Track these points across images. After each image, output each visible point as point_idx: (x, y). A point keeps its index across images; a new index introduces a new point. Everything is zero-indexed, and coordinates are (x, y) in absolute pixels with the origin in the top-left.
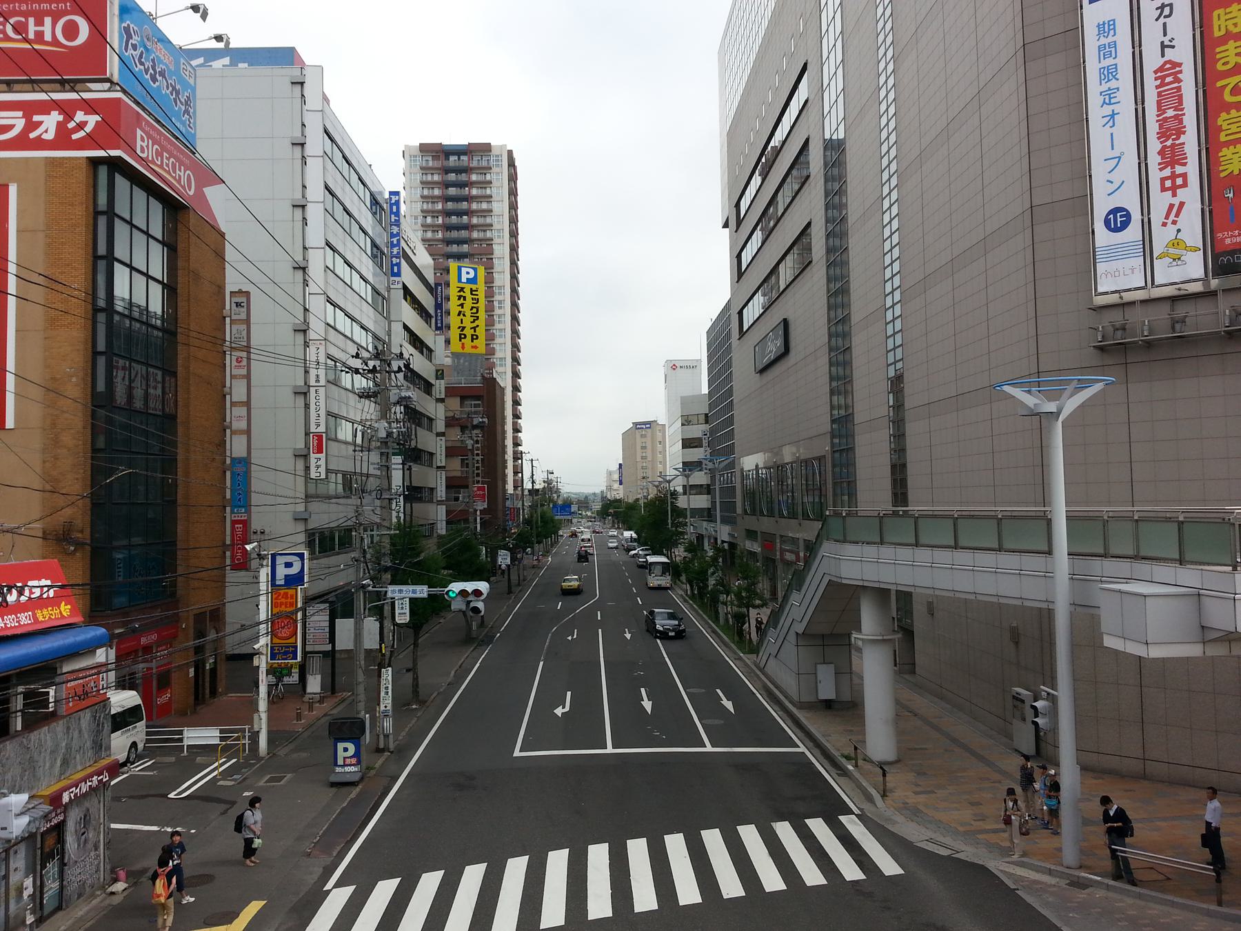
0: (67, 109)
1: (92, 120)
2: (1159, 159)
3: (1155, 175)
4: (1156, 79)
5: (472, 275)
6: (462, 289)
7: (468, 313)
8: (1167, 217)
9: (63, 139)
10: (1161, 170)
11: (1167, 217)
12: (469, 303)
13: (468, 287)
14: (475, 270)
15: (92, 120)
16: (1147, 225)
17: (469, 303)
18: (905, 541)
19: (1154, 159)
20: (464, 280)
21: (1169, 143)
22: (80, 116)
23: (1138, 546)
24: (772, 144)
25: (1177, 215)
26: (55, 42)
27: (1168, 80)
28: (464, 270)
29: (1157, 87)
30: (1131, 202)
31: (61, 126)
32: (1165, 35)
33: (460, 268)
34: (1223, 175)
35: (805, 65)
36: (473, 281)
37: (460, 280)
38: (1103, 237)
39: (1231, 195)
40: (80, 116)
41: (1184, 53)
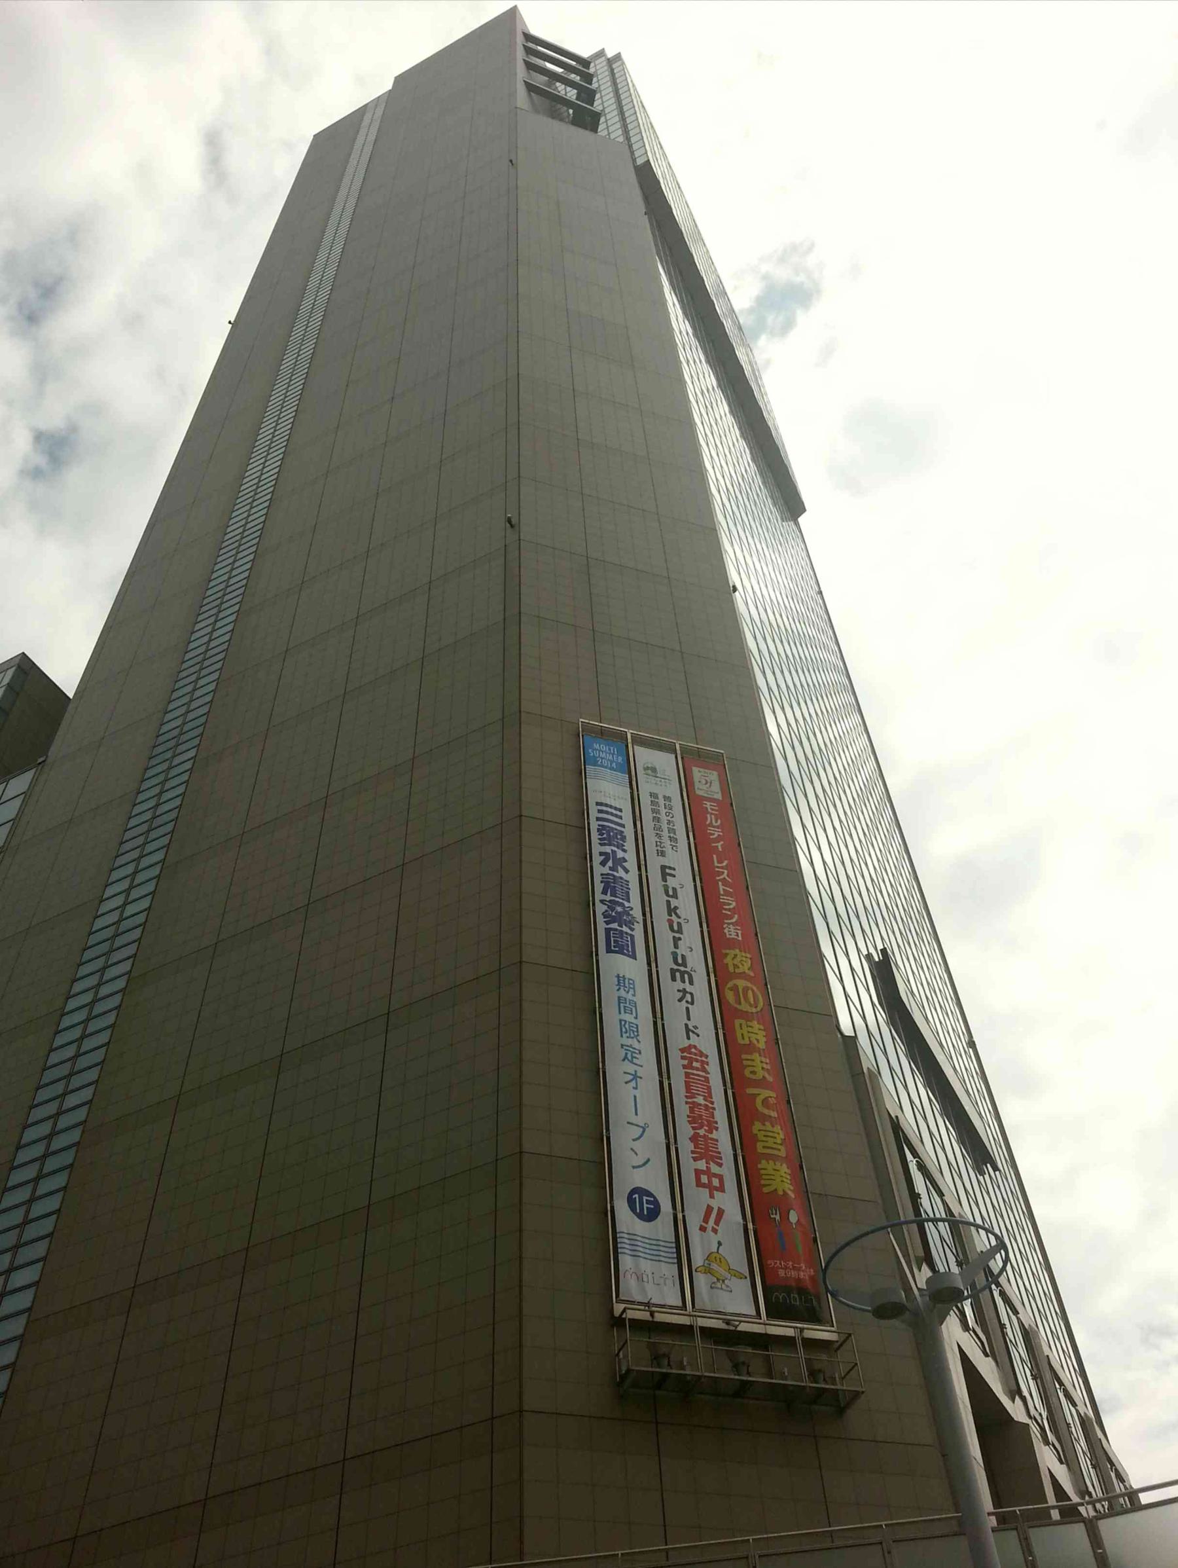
2: (691, 1146)
3: (689, 1166)
4: (683, 1058)
8: (706, 1220)
10: (695, 1159)
11: (706, 1220)
16: (679, 1224)
18: (790, 1549)
19: (686, 1147)
21: (702, 1132)
25: (717, 1222)
27: (695, 1064)
29: (684, 1067)
30: (656, 1182)
32: (689, 1019)
34: (766, 1190)
35: (648, 1160)
38: (626, 1220)
39: (778, 1217)
41: (706, 1042)
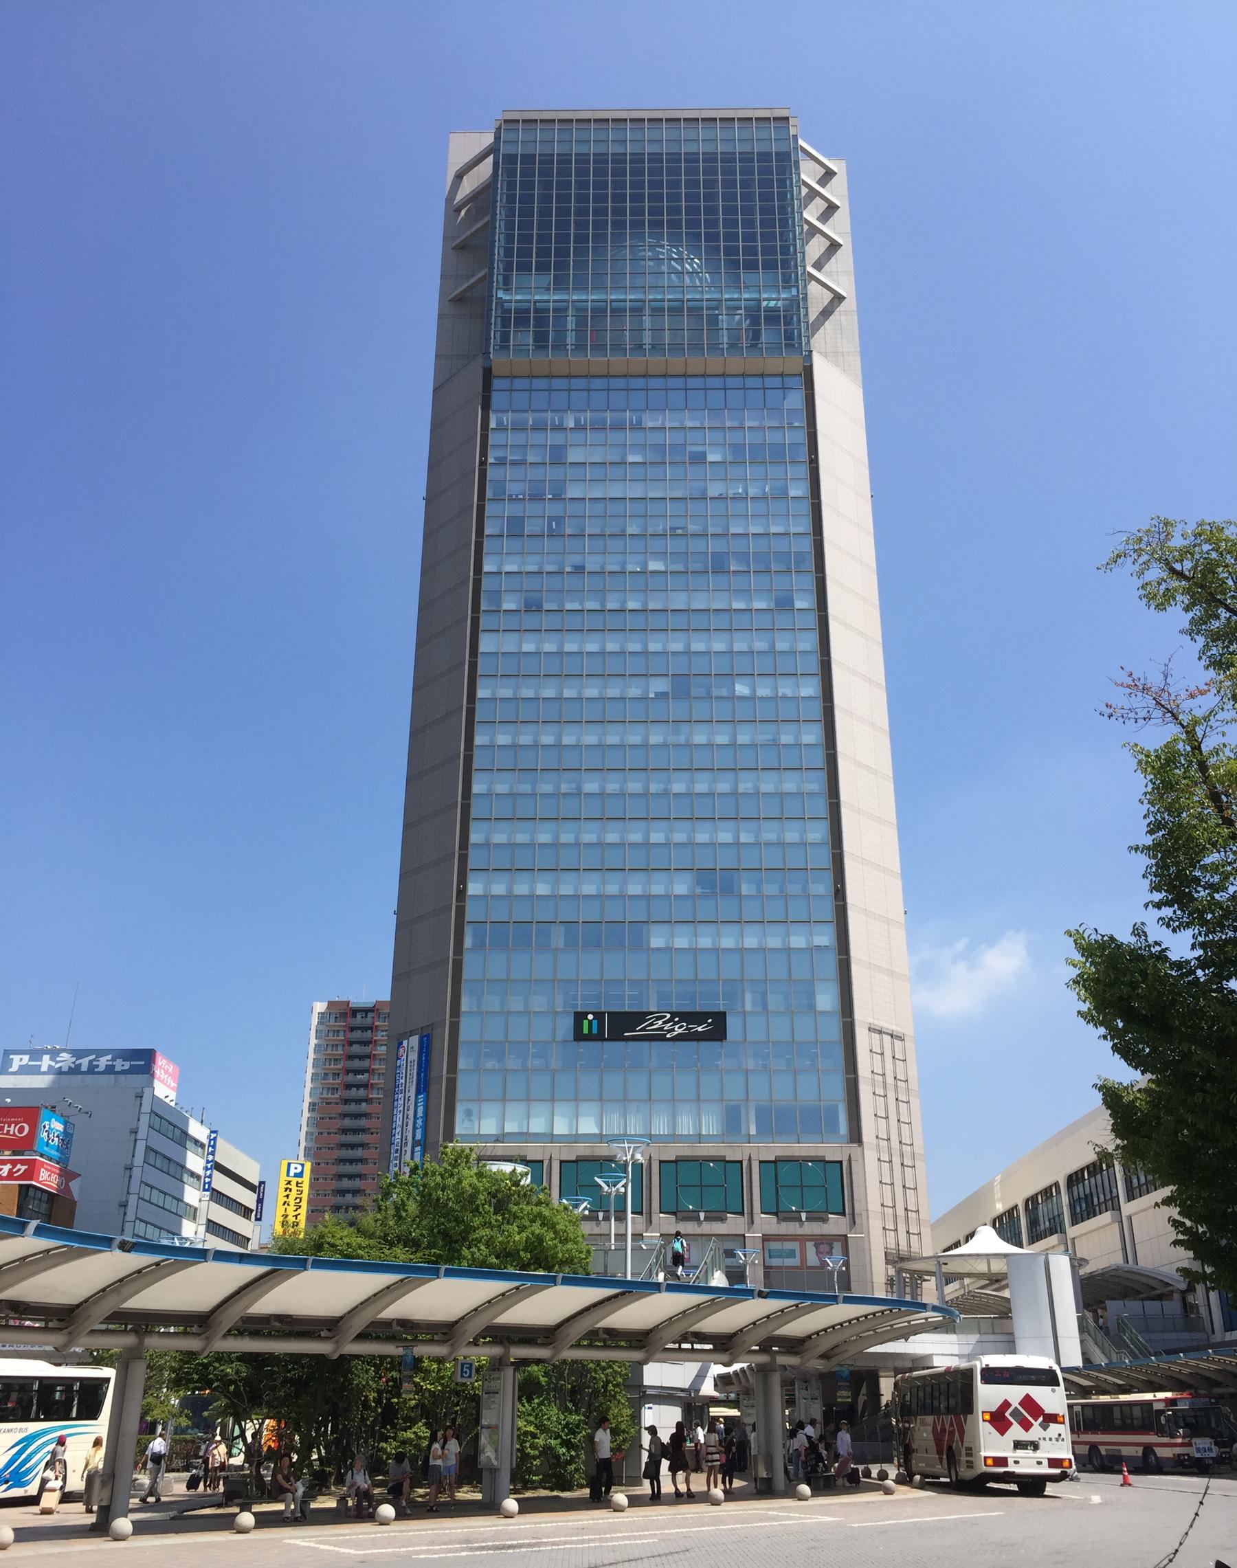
0: (14, 1163)
1: (24, 1168)
5: (299, 1170)
6: (289, 1183)
7: (292, 1203)
9: (10, 1176)
12: (294, 1194)
13: (294, 1180)
14: (303, 1165)
15: (24, 1168)
17: (294, 1194)
20: (292, 1174)
22: (19, 1166)
23: (768, 1033)
24: (1122, 1448)
26: (14, 1135)
28: (293, 1166)
31: (10, 1170)
33: (289, 1164)
36: (300, 1175)
37: (288, 1175)
40: (19, 1166)
